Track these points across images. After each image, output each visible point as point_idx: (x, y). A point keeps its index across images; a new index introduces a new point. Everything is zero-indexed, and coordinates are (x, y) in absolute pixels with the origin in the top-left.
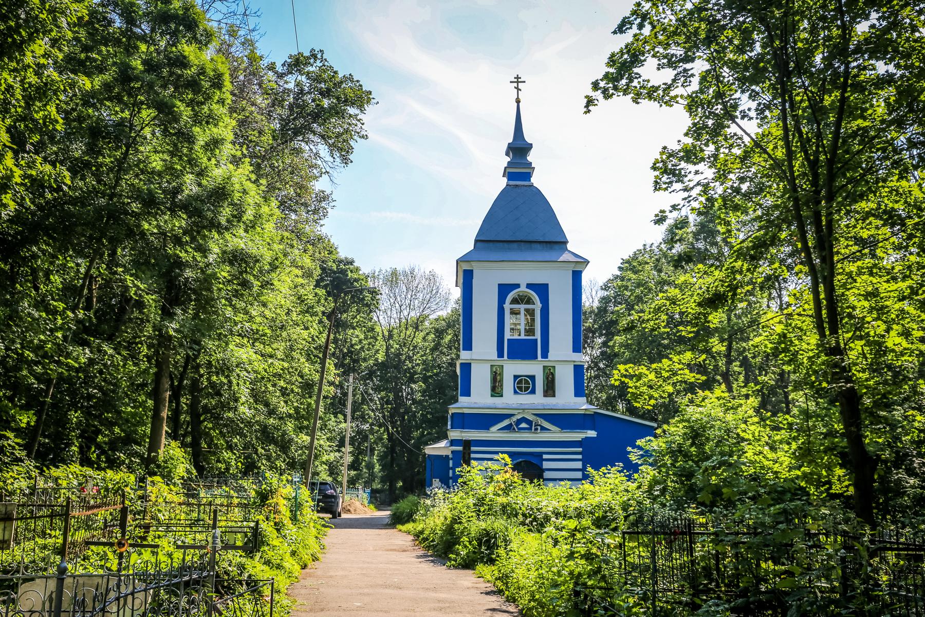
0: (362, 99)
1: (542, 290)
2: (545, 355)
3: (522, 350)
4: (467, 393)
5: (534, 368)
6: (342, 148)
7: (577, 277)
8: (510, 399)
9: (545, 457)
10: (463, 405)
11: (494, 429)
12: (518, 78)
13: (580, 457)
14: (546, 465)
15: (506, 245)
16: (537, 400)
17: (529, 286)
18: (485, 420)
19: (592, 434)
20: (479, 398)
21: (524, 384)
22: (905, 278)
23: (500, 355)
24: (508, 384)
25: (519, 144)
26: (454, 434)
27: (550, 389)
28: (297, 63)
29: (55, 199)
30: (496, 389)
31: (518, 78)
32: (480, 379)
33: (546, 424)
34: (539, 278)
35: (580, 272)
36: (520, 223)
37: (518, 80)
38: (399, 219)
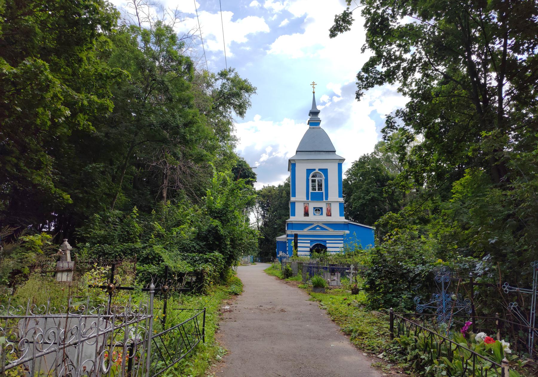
0: (249, 89)
1: (325, 171)
2: (327, 198)
3: (317, 197)
4: (294, 215)
5: (323, 205)
6: (241, 110)
7: (340, 166)
8: (313, 218)
9: (327, 242)
10: (292, 219)
11: (306, 230)
12: (314, 83)
13: (342, 242)
14: (328, 245)
15: (309, 153)
16: (324, 218)
17: (320, 170)
18: (302, 226)
19: (347, 232)
20: (298, 217)
21: (318, 210)
22: (388, 140)
23: (308, 198)
24: (311, 211)
25: (314, 110)
26: (289, 232)
27: (329, 214)
28: (223, 75)
29: (464, 110)
30: (306, 214)
31: (314, 83)
32: (299, 209)
33: (327, 228)
34: (323, 166)
35: (341, 164)
36: (316, 145)
37: (314, 84)
38: (264, 141)
